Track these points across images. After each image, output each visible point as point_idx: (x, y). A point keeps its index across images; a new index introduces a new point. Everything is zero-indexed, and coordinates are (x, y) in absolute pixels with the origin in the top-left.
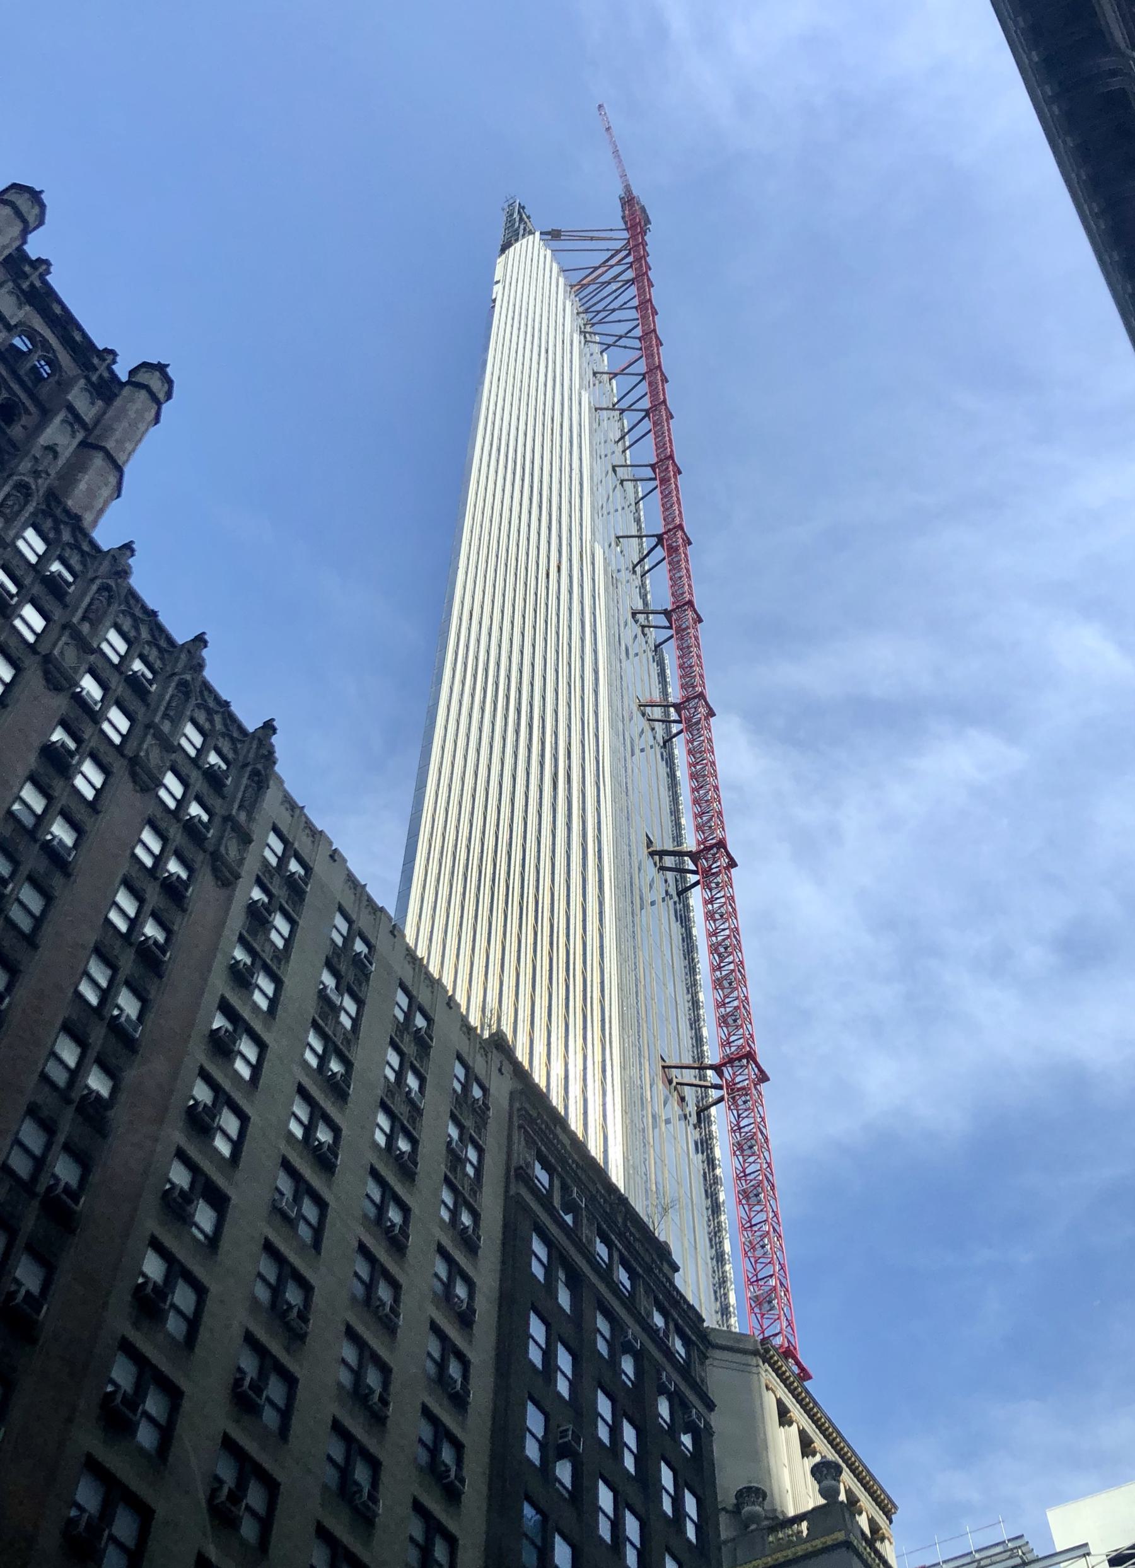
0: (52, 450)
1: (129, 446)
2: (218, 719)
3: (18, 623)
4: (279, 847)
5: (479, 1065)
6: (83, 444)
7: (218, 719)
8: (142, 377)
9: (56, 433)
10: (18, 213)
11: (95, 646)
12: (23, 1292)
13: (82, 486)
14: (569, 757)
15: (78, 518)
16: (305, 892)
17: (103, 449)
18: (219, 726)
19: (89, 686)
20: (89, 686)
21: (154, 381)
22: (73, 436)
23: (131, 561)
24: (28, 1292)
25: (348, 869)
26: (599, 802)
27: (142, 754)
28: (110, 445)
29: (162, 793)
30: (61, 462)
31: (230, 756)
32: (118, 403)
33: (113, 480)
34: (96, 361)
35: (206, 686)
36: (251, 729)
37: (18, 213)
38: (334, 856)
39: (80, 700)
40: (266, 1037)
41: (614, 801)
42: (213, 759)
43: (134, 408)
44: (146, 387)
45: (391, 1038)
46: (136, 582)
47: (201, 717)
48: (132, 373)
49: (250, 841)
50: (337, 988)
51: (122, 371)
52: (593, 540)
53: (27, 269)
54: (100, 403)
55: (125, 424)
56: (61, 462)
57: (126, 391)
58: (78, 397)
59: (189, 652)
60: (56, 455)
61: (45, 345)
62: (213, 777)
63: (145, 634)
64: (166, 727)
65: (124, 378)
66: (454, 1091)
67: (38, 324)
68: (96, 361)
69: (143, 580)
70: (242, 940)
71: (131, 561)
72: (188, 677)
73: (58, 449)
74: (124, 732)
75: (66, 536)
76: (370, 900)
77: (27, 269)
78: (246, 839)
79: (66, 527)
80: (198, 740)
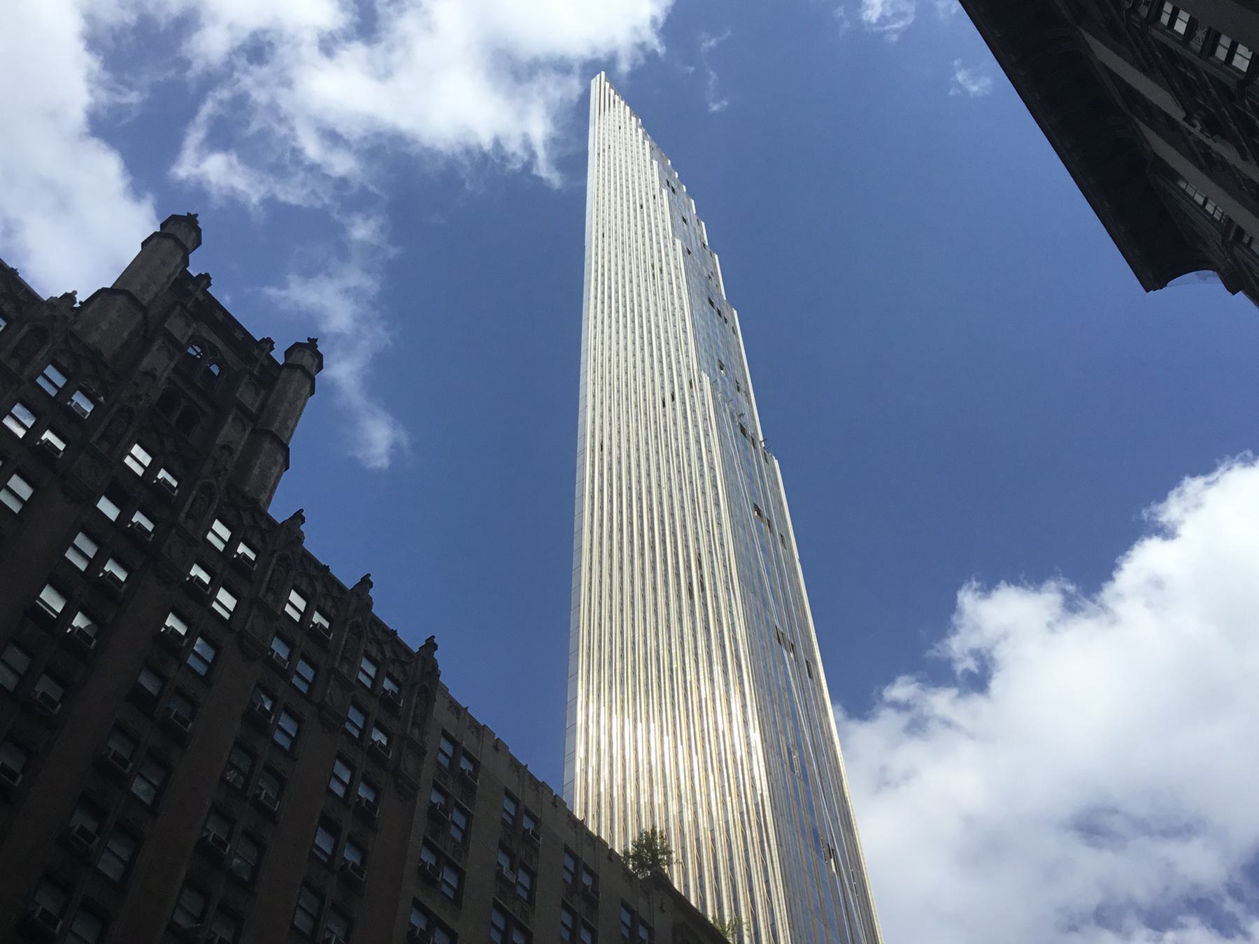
0: (226, 447)
1: (290, 423)
2: (387, 649)
3: (215, 605)
4: (449, 749)
5: (642, 908)
6: (254, 431)
7: (387, 649)
8: (296, 358)
9: (231, 433)
10: (178, 242)
11: (279, 613)
12: (39, 911)
13: (256, 471)
14: (701, 567)
15: (255, 502)
16: (476, 787)
17: (270, 433)
18: (389, 654)
19: (279, 649)
20: (279, 649)
21: (307, 360)
22: (244, 430)
23: (302, 528)
24: (44, 911)
25: (510, 755)
26: (730, 605)
27: (327, 699)
28: (275, 427)
29: (348, 726)
30: (236, 457)
31: (401, 678)
32: (279, 385)
33: (280, 459)
34: (256, 352)
35: (377, 623)
36: (416, 650)
37: (178, 242)
38: (498, 746)
39: (271, 663)
40: (455, 926)
41: (744, 602)
42: (387, 685)
43: (428, 772)
44: (301, 367)
45: (563, 901)
46: (311, 545)
47: (374, 652)
48: (288, 353)
49: (424, 753)
50: (511, 866)
51: (278, 356)
52: (699, 370)
53: (191, 287)
54: (263, 392)
55: (286, 405)
56: (236, 457)
57: (284, 374)
58: (247, 396)
59: (358, 595)
60: (231, 452)
61: (214, 350)
62: (388, 703)
63: (319, 588)
64: (345, 669)
65: (281, 361)
66: (623, 936)
67: (206, 333)
68: (256, 352)
69: (315, 543)
70: (427, 843)
71: (302, 528)
72: (359, 619)
73: (233, 446)
74: (310, 679)
75: (247, 520)
76: (531, 776)
77: (191, 287)
78: (421, 753)
79: (249, 517)
80: (371, 671)
